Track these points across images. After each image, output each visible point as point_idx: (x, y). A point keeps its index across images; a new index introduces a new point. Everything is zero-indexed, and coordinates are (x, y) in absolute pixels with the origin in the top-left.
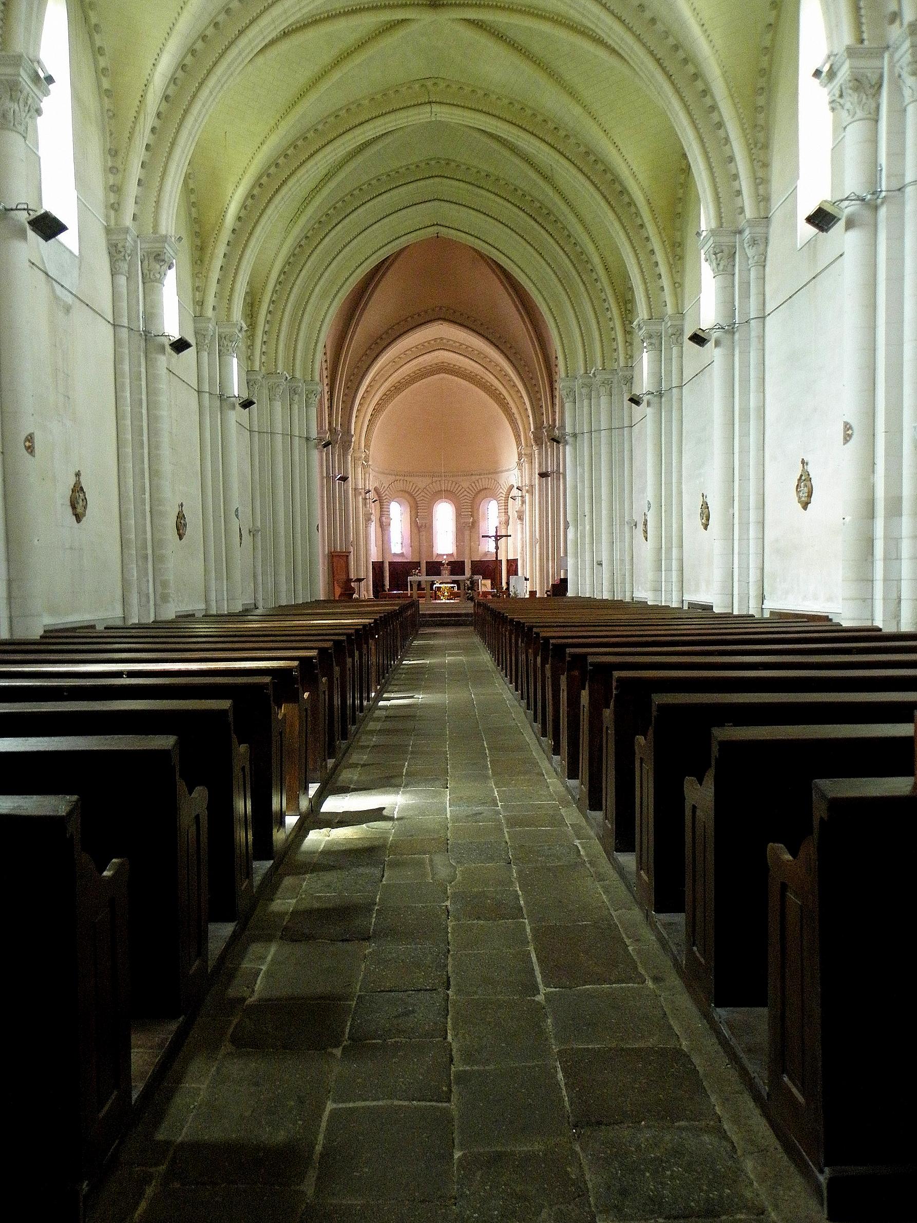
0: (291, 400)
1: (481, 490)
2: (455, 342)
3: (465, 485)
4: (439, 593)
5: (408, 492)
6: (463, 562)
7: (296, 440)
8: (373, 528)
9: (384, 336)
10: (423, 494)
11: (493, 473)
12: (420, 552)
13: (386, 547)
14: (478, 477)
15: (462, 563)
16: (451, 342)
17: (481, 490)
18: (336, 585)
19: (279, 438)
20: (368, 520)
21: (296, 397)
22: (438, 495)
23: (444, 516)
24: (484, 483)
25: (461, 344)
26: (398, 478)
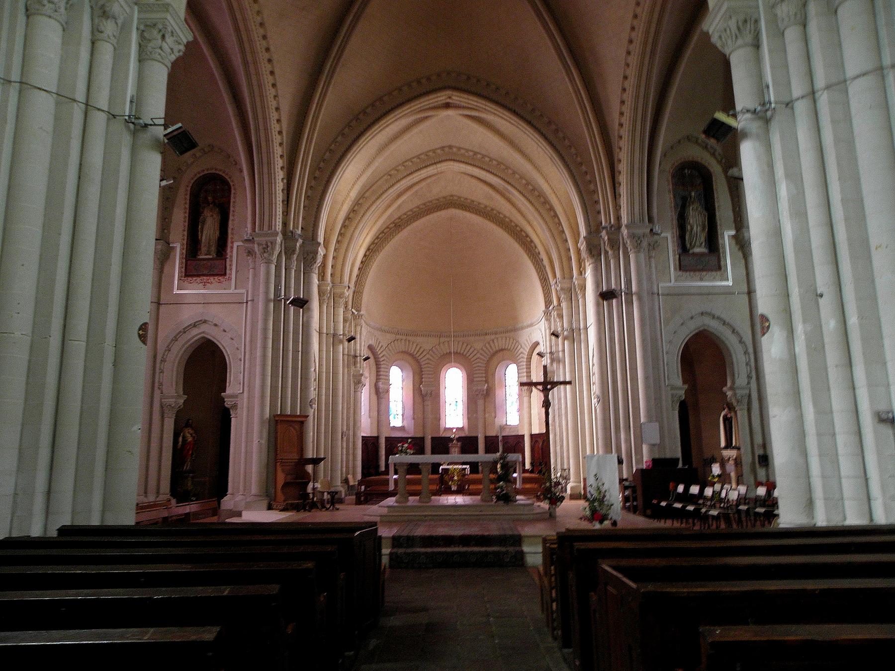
0: (96, 31)
1: (497, 352)
2: (467, 150)
3: (478, 346)
4: (446, 477)
5: (412, 355)
6: (476, 438)
7: (99, 121)
8: (365, 395)
9: (369, 110)
11: (511, 331)
12: (424, 427)
13: (383, 418)
14: (493, 337)
15: (475, 439)
16: (463, 151)
18: (279, 469)
19: (42, 108)
20: (358, 383)
21: (109, 28)
22: (446, 359)
23: (454, 383)
24: (500, 343)
25: (475, 153)
26: (398, 337)
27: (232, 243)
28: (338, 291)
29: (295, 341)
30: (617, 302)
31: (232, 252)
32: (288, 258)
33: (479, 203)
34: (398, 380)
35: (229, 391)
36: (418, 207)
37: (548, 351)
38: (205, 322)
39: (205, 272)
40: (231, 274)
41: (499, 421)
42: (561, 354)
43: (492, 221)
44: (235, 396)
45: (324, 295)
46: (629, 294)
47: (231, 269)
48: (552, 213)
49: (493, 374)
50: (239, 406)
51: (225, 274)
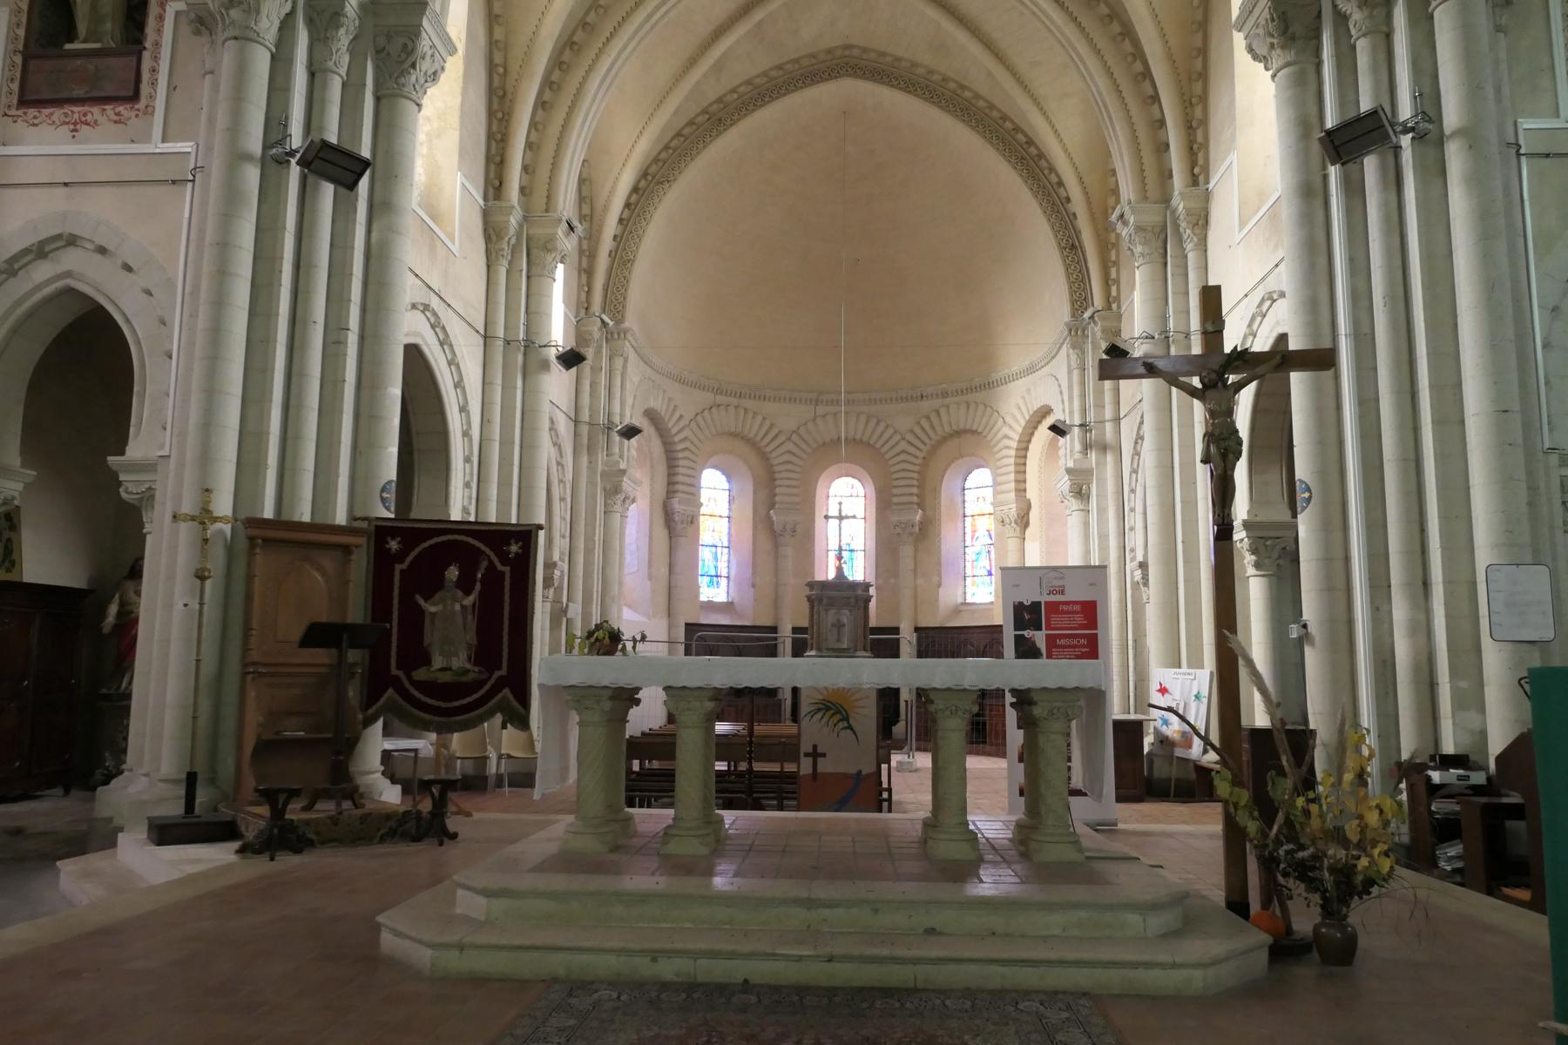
10: (789, 446)
12: (776, 603)
14: (936, 403)
17: (945, 439)
20: (613, 488)
22: (831, 453)
26: (720, 399)
27: (162, 5)
28: (539, 231)
29: (337, 298)
30: (1383, 168)
31: (159, 31)
32: (320, 40)
33: (914, 65)
34: (716, 495)
35: (137, 449)
36: (765, 74)
37: (1077, 421)
38: (72, 241)
39: (78, 92)
40: (152, 97)
41: (949, 596)
42: (1109, 427)
43: (945, 109)
44: (148, 467)
45: (500, 237)
46: (1428, 131)
47: (154, 84)
48: (1116, 28)
49: (936, 491)
50: (157, 497)
51: (135, 97)
